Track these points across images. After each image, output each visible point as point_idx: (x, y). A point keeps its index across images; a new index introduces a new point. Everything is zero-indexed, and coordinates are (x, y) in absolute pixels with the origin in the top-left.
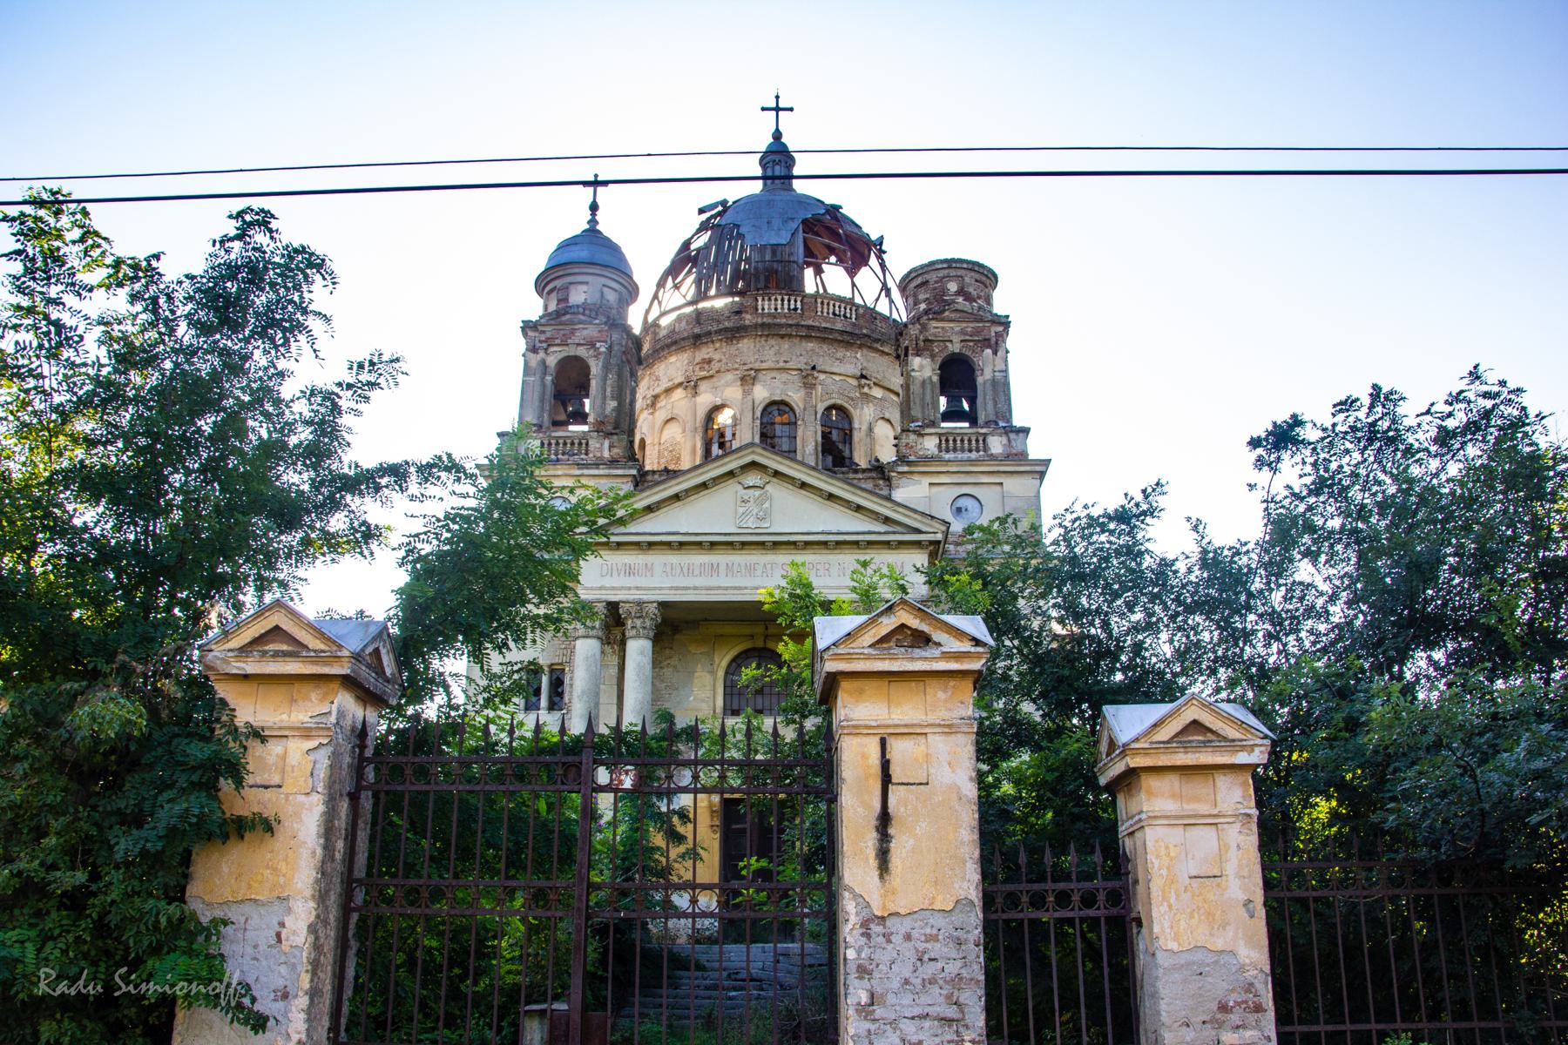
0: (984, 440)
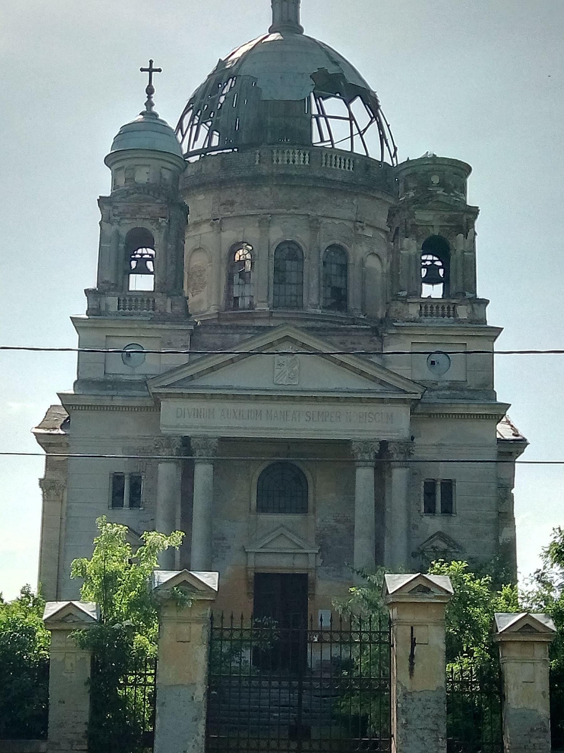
0: (454, 308)
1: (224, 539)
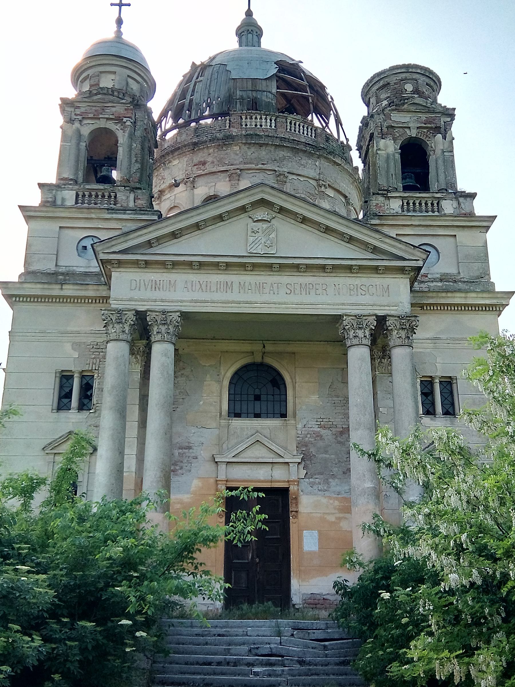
1: (189, 448)
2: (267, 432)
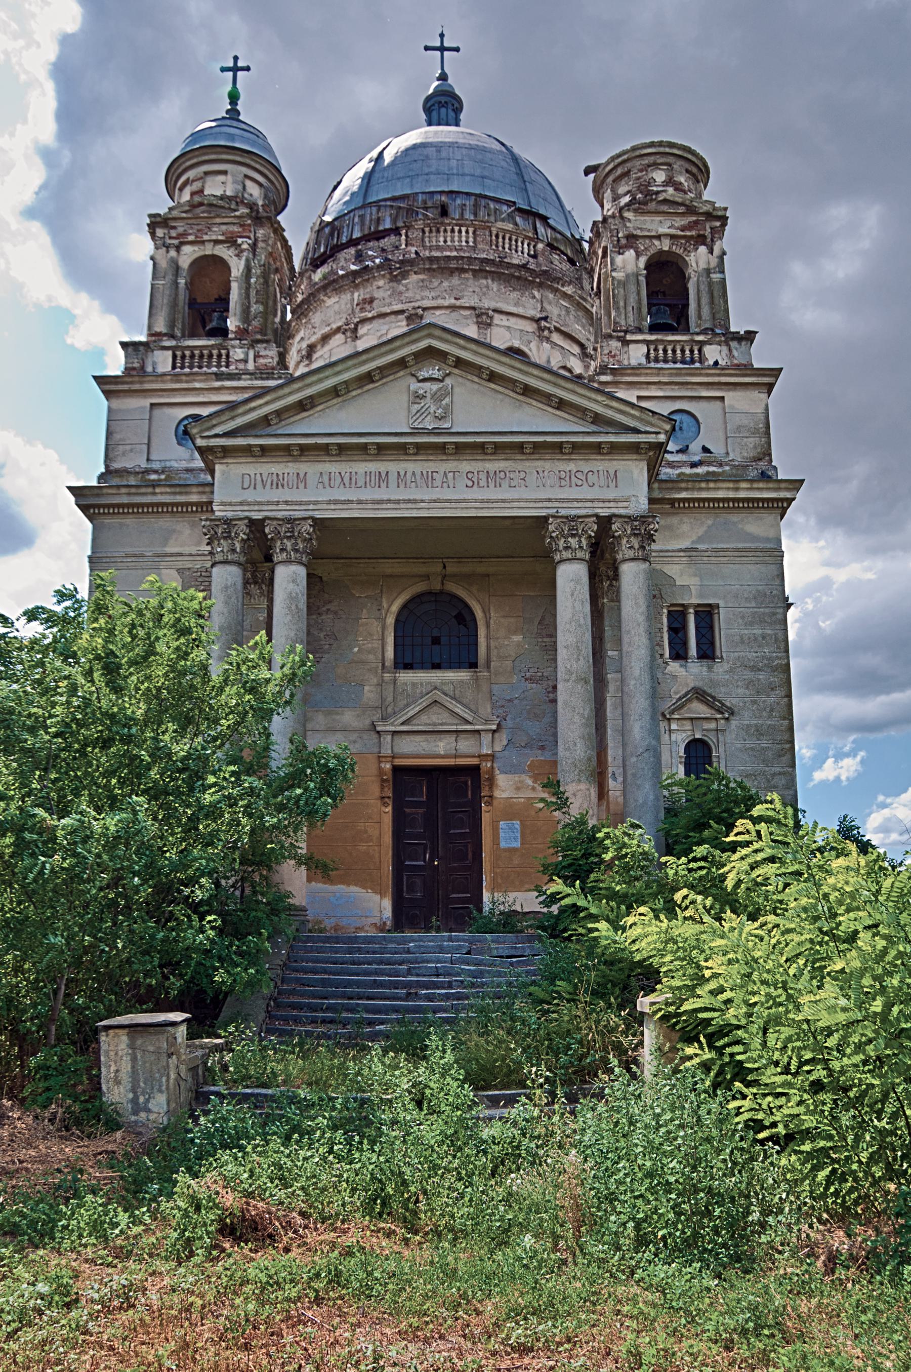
0: (700, 351)
2: (449, 689)
